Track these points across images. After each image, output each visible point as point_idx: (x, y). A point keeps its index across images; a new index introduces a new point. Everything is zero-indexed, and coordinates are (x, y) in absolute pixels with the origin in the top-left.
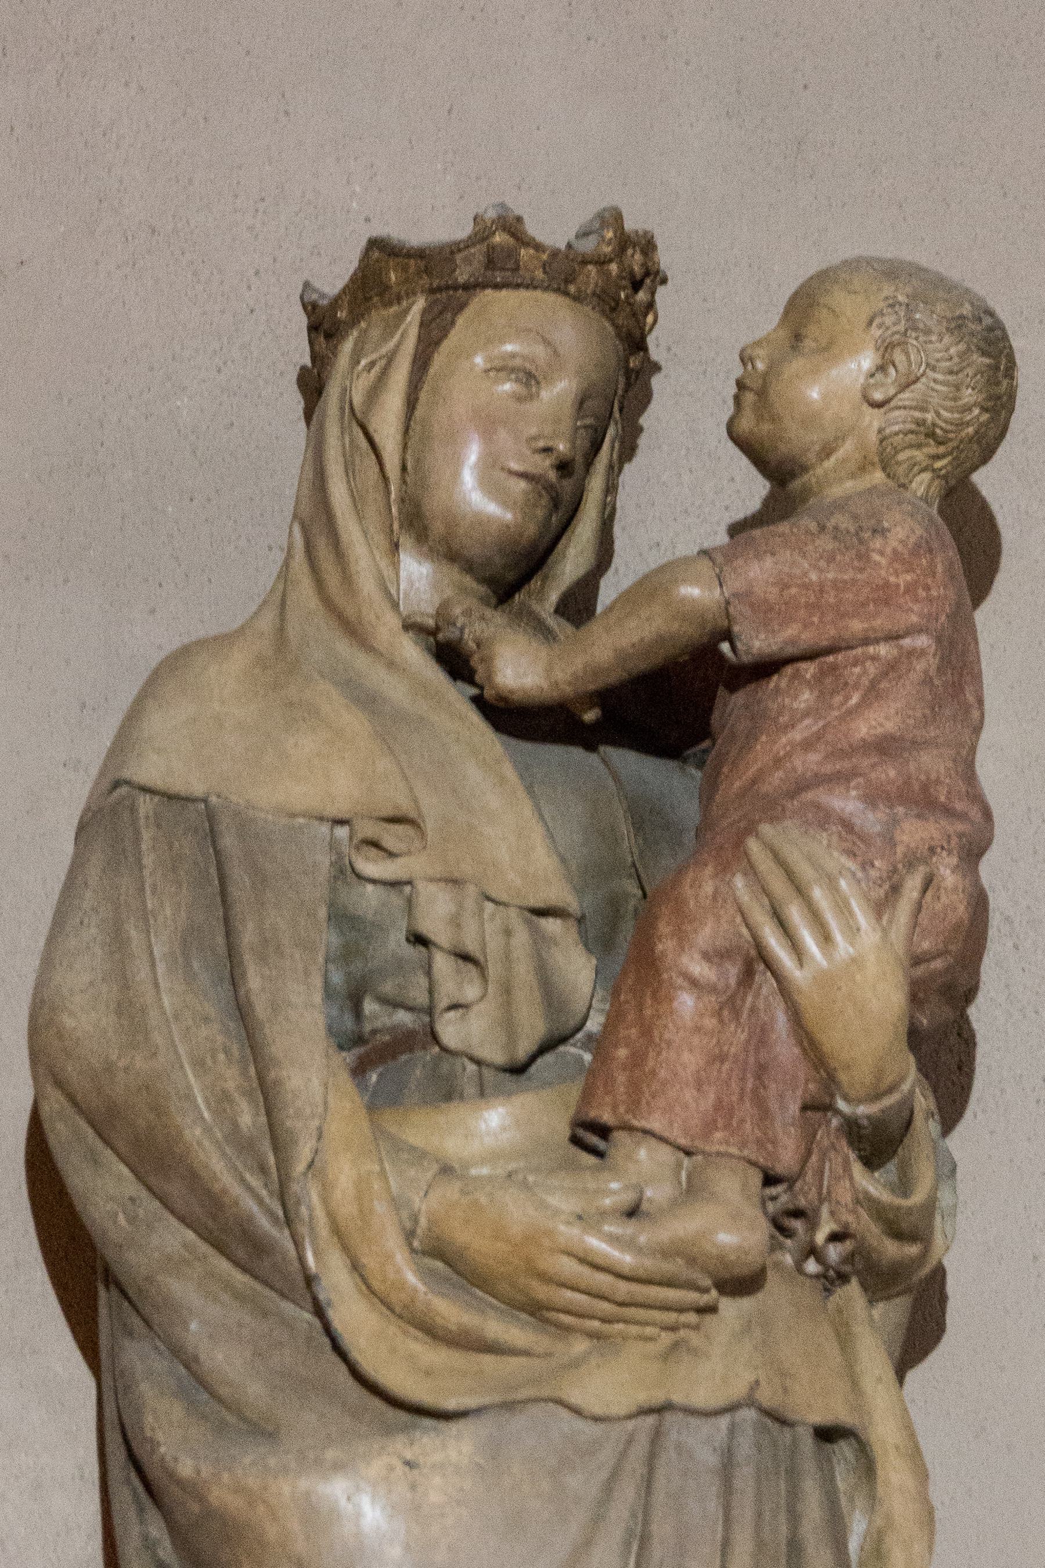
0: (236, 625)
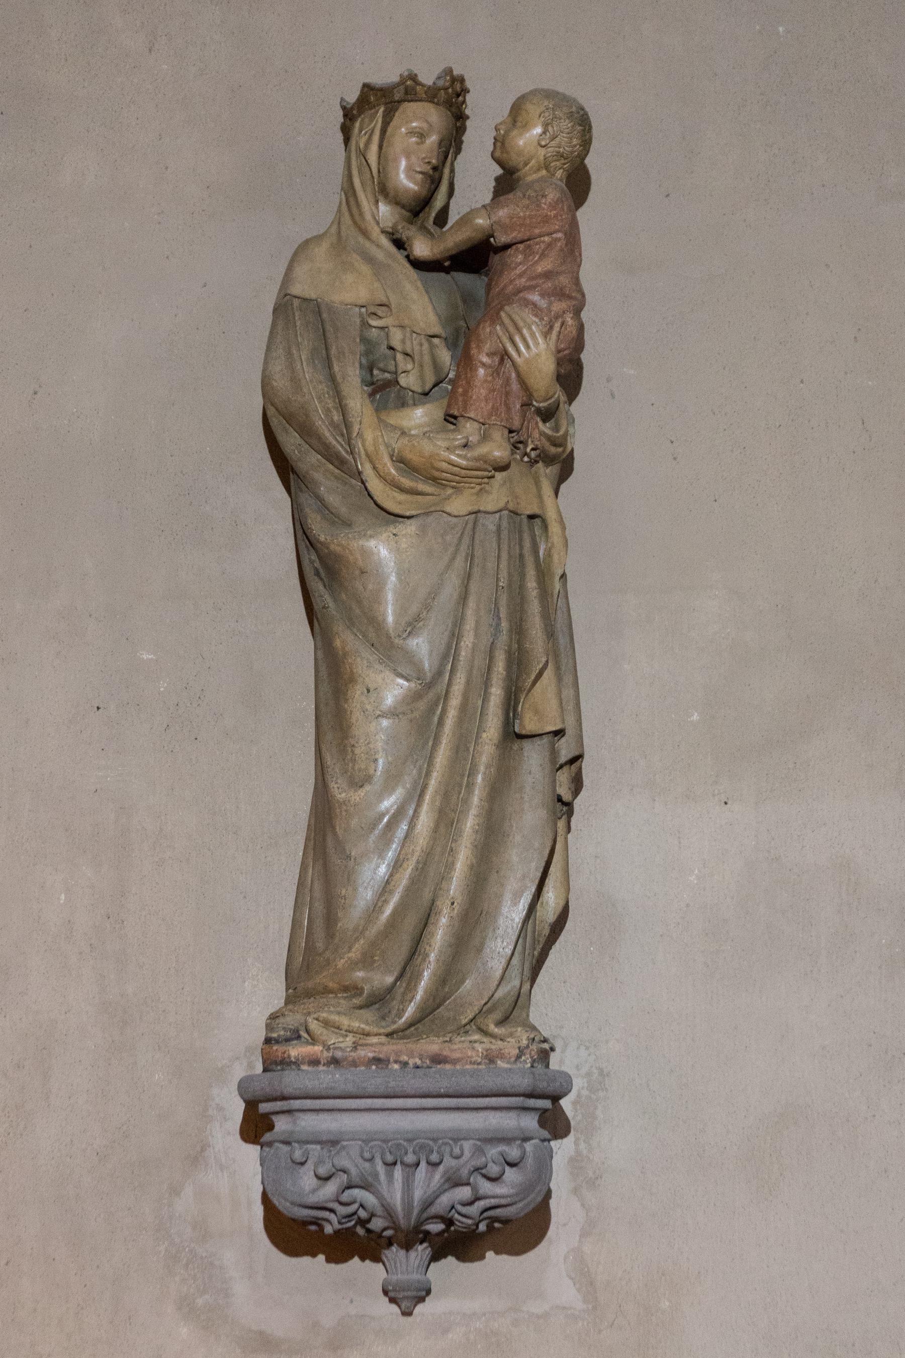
0: (321, 232)
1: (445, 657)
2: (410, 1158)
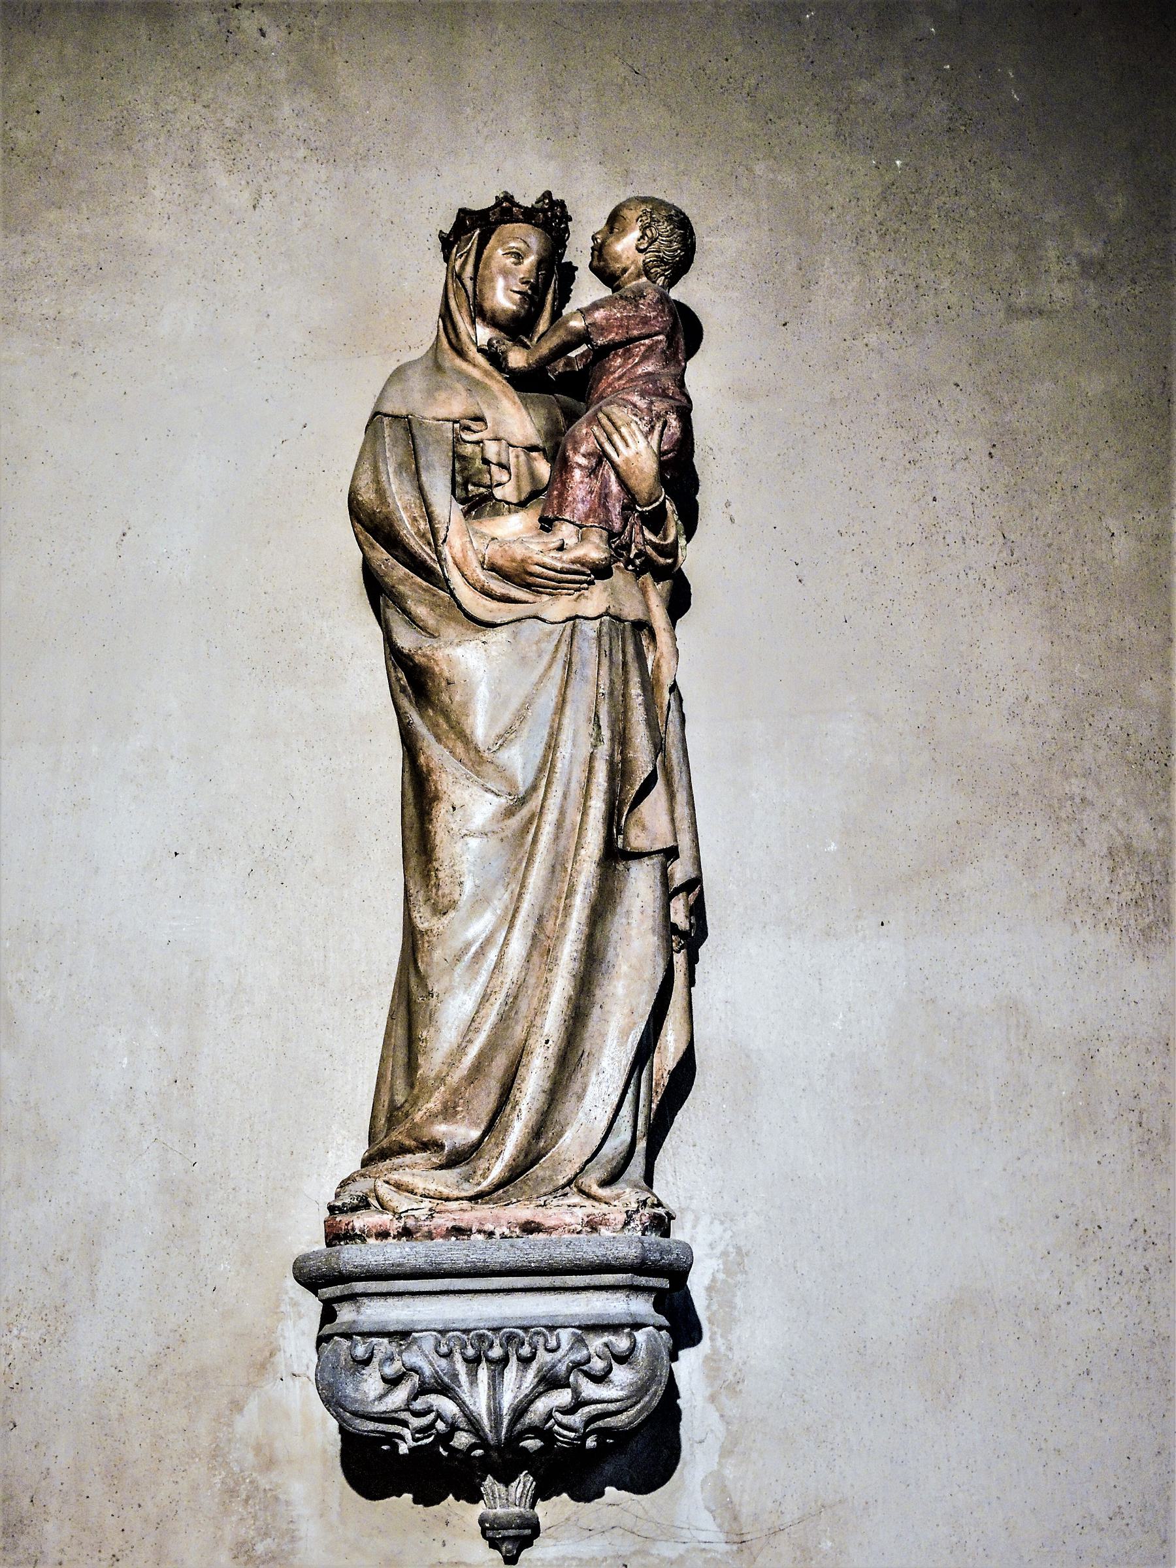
1: (541, 770)
2: (496, 1352)
